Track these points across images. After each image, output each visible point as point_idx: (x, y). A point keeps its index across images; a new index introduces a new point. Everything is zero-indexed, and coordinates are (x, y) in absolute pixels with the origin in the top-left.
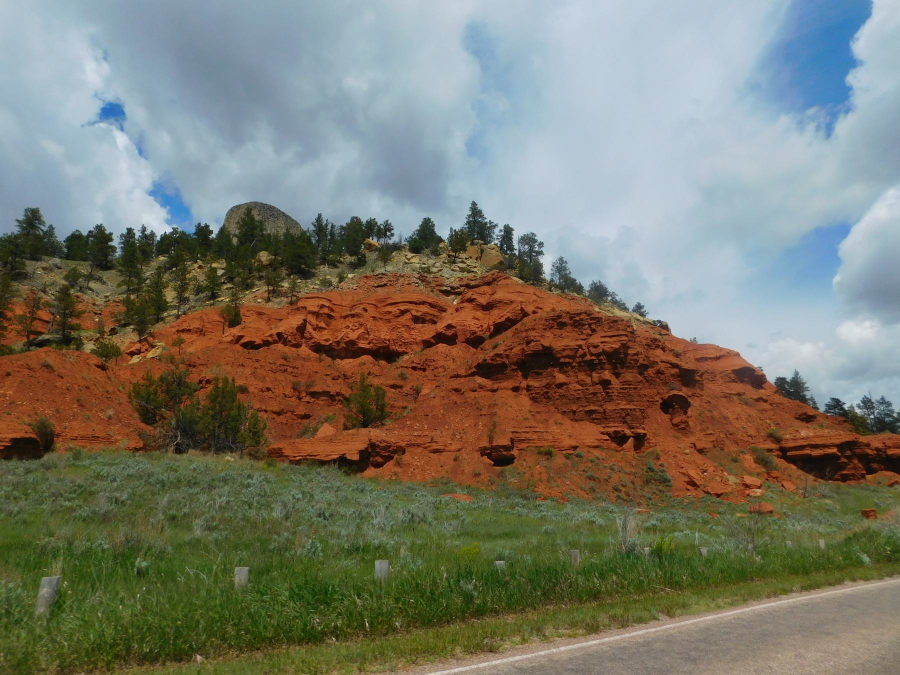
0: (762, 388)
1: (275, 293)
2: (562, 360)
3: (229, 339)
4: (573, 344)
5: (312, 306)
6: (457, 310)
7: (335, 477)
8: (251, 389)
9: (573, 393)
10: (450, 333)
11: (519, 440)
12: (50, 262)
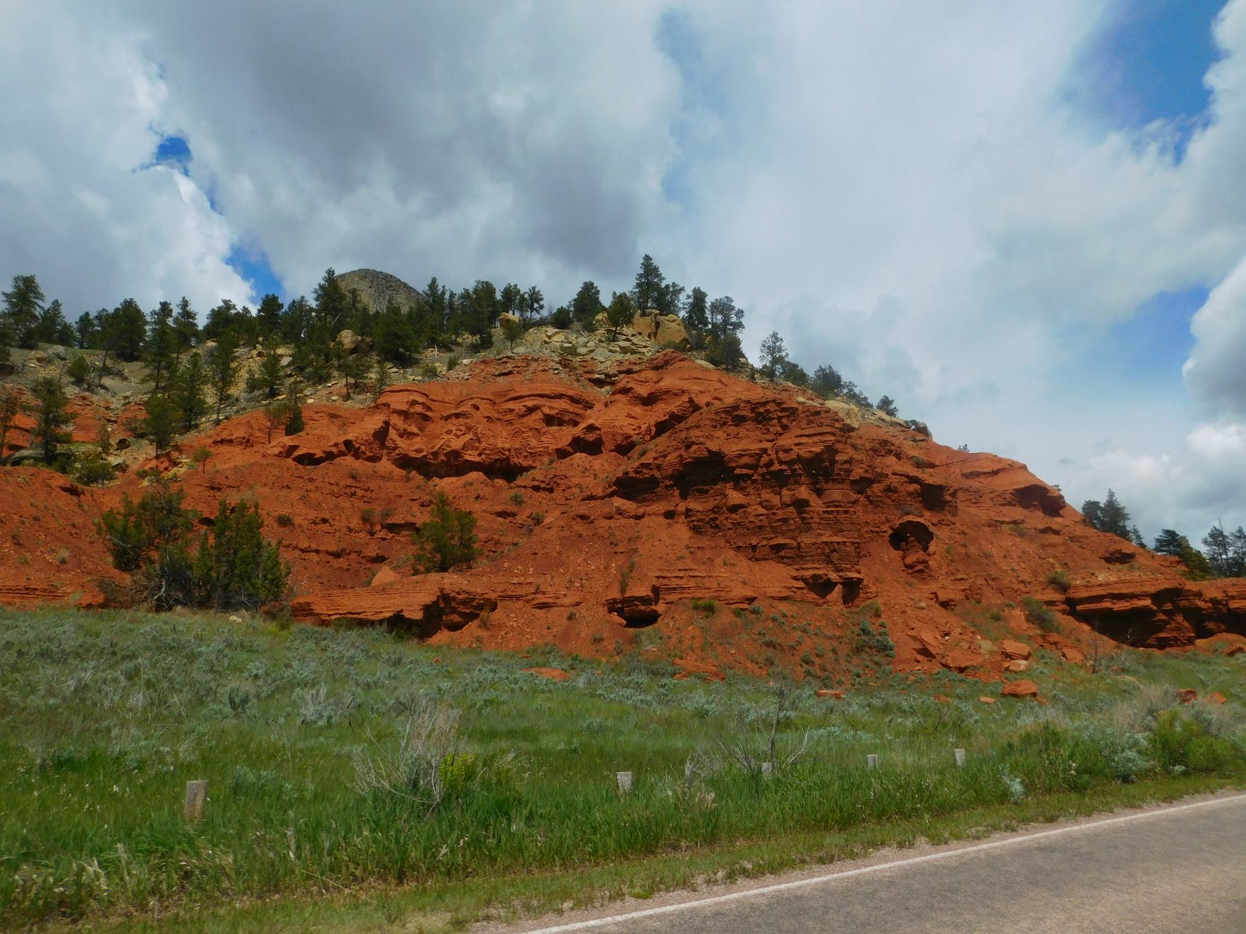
0: (1059, 515)
1: (358, 387)
2: (738, 471)
3: (276, 451)
4: (754, 447)
5: (399, 402)
6: (606, 405)
7: (388, 647)
8: (297, 520)
9: (753, 519)
10: (591, 437)
11: (668, 589)
12: (50, 351)
